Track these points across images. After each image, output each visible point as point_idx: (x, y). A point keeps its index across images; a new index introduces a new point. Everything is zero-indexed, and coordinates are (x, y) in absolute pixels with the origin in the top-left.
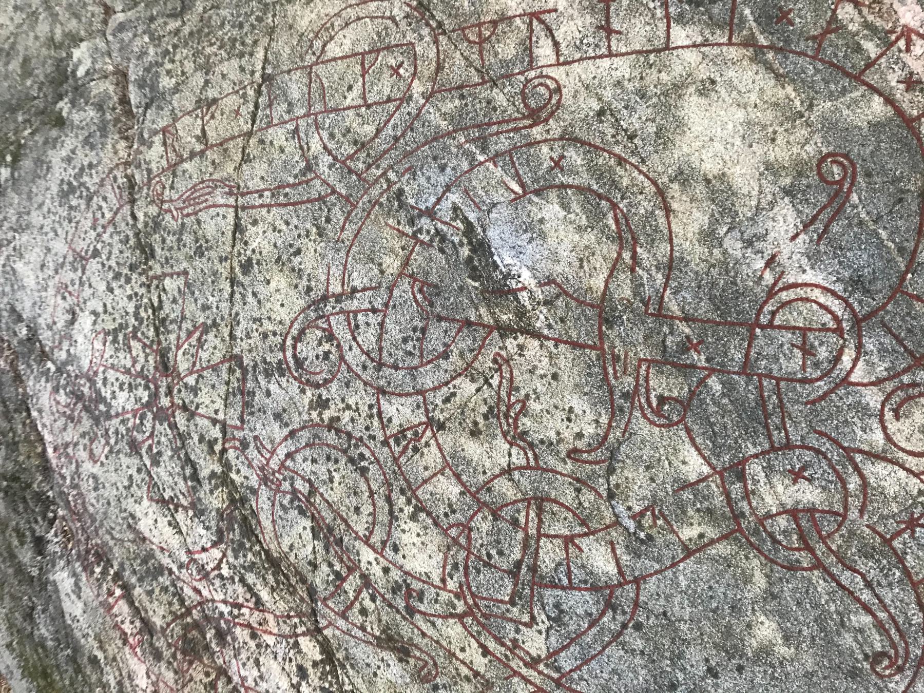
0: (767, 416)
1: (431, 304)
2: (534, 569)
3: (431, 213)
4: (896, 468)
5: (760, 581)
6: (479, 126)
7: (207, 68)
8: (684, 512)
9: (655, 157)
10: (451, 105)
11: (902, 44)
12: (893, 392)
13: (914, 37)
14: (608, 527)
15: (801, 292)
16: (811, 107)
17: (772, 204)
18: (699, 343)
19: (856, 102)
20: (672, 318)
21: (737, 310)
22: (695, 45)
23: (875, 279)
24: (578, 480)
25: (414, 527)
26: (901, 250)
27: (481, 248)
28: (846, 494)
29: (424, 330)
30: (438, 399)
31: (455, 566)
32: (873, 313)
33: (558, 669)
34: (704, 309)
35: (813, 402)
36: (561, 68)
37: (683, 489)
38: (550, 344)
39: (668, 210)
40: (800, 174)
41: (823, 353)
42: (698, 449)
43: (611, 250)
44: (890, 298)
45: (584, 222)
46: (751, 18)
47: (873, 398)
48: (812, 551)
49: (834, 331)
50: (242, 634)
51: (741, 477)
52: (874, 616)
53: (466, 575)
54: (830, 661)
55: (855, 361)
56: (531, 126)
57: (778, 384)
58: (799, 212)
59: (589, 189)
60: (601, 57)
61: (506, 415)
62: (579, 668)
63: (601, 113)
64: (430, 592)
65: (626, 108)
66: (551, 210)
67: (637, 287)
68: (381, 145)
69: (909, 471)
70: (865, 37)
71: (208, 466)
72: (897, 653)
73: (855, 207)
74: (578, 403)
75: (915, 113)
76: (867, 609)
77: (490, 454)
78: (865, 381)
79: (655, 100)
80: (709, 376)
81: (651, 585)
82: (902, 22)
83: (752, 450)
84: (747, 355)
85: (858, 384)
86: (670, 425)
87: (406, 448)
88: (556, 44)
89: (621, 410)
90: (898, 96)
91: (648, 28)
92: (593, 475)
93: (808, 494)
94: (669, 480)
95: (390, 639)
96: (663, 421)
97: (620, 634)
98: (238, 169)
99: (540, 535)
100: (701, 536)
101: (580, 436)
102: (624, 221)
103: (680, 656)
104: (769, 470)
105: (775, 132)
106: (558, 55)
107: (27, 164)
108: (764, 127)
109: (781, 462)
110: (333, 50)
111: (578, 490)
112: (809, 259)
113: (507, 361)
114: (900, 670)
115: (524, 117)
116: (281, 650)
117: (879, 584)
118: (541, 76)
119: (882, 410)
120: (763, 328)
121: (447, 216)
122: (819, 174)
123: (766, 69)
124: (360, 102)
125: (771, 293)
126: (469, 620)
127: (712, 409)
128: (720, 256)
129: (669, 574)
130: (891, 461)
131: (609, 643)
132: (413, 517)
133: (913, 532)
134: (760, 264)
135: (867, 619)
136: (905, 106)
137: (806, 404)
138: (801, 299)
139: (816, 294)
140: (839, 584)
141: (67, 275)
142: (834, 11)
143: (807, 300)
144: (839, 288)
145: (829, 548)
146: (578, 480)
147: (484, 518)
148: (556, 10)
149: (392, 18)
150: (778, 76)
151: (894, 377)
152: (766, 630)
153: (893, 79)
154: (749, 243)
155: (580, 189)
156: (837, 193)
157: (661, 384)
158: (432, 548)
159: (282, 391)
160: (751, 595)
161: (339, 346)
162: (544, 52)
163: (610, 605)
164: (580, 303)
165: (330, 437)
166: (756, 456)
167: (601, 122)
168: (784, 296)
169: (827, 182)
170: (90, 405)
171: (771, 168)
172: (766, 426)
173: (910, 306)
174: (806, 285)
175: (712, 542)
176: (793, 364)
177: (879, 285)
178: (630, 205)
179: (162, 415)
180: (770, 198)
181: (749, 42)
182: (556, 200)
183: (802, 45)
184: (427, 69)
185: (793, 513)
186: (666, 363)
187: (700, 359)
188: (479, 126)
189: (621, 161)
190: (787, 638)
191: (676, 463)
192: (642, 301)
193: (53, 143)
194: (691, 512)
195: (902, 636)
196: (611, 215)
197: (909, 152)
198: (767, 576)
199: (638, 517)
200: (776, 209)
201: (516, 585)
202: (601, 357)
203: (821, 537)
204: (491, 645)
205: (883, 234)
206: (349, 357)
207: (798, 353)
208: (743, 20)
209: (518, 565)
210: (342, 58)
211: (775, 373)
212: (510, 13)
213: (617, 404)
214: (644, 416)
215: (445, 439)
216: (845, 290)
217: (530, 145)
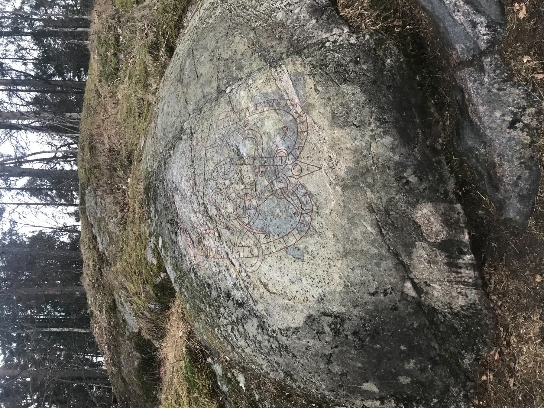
3: (232, 146)
5: (276, 202)
7: (203, 124)
10: (235, 126)
21: (273, 155)
25: (229, 203)
27: (239, 150)
30: (232, 179)
34: (267, 156)
41: (284, 160)
43: (255, 147)
47: (290, 167)
51: (273, 184)
66: (247, 142)
68: (225, 134)
71: (201, 201)
74: (250, 175)
77: (239, 187)
81: (261, 206)
93: (282, 185)
102: (256, 142)
107: (176, 149)
110: (220, 118)
121: (234, 145)
125: (277, 151)
139: (283, 150)
141: (181, 170)
155: (251, 138)
157: (262, 169)
159: (211, 183)
162: (248, 114)
165: (218, 190)
170: (184, 196)
171: (276, 130)
176: (279, 163)
179: (195, 194)
181: (275, 109)
184: (232, 120)
185: (280, 189)
187: (266, 164)
193: (180, 144)
199: (259, 194)
204: (241, 223)
215: (233, 186)
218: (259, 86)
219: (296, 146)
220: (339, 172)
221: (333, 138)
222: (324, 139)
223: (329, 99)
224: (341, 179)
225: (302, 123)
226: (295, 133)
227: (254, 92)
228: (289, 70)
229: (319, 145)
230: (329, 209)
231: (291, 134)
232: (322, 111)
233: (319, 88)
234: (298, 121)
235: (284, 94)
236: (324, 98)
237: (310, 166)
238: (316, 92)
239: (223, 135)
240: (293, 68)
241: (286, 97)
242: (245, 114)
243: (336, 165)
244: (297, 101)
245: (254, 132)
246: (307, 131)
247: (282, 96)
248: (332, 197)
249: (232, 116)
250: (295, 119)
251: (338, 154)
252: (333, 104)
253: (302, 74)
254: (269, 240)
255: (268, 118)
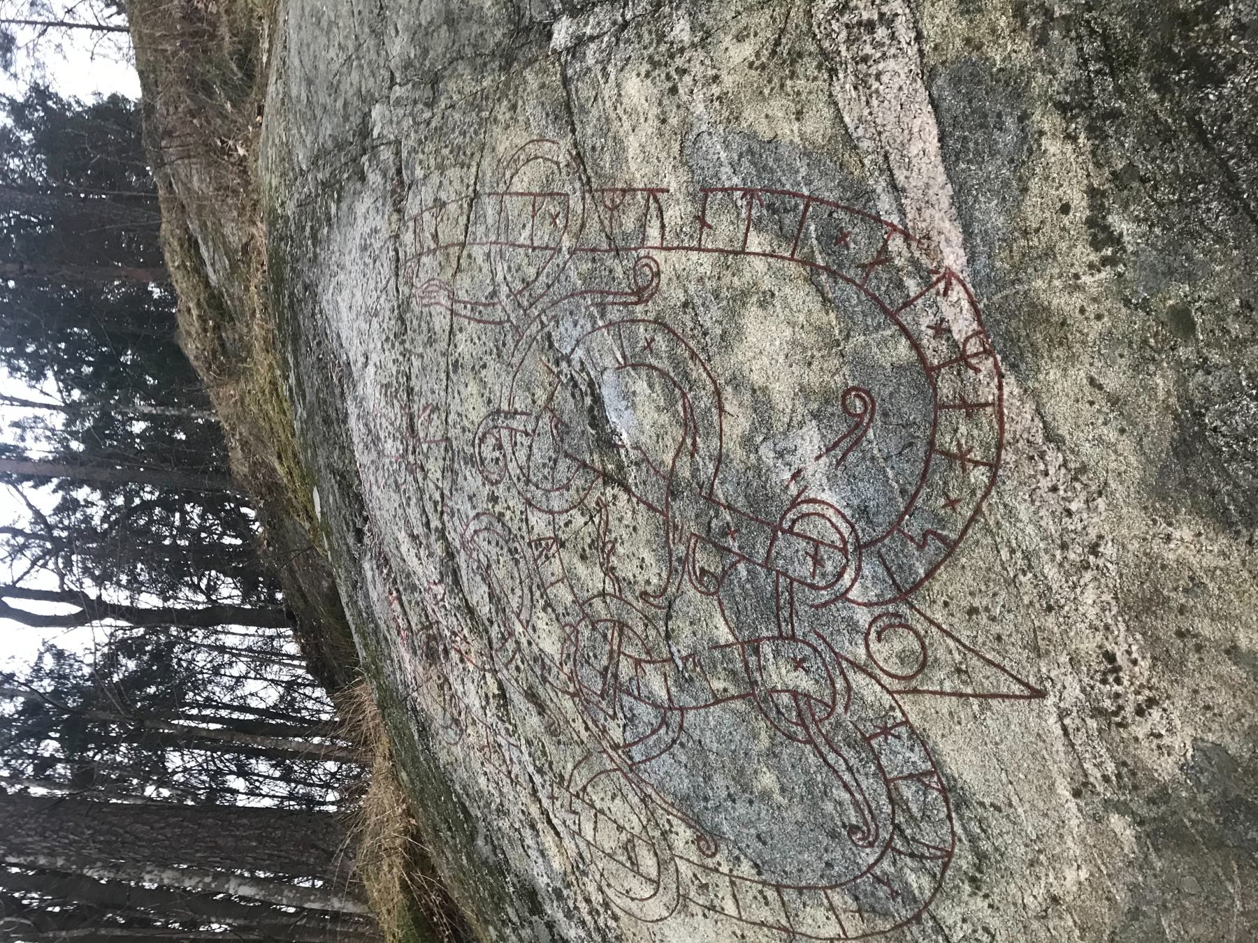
0: (779, 608)
1: (562, 440)
2: (615, 676)
4: (873, 681)
5: (764, 741)
6: (602, 292)
8: (715, 667)
9: (717, 357)
10: (586, 267)
11: (941, 286)
12: (880, 616)
13: (954, 282)
14: (664, 661)
15: (818, 508)
16: (848, 336)
17: (801, 425)
18: (736, 531)
19: (885, 341)
20: (719, 504)
21: (768, 513)
22: (764, 255)
23: (878, 513)
24: (646, 617)
26: (903, 492)
28: (834, 692)
29: (555, 461)
31: (568, 656)
32: (873, 543)
33: (631, 758)
34: (740, 503)
35: (817, 607)
36: (663, 253)
37: (715, 648)
38: (635, 500)
39: (721, 409)
40: (827, 402)
41: (829, 567)
42: (725, 620)
43: (679, 433)
44: (889, 533)
45: (662, 403)
46: (814, 235)
47: (863, 617)
48: (807, 728)
49: (840, 550)
50: (454, 656)
51: (756, 652)
52: (852, 794)
53: (575, 665)
54: (815, 818)
55: (854, 581)
56: (636, 303)
57: (791, 583)
58: (823, 436)
59: (668, 375)
60: (692, 249)
61: (601, 548)
62: (644, 762)
63: (685, 305)
64: (555, 670)
65: (703, 305)
67: (695, 471)
69: (883, 686)
70: (909, 274)
72: (869, 830)
73: (870, 442)
75: (936, 362)
76: (846, 786)
77: (592, 578)
78: (860, 600)
79: (725, 303)
80: (739, 561)
82: (946, 263)
83: (765, 634)
84: (769, 552)
85: (853, 602)
86: (708, 594)
87: (541, 553)
88: (663, 227)
89: (676, 571)
90: (925, 341)
91: (731, 228)
92: (655, 616)
93: (805, 683)
94: (706, 638)
95: (533, 695)
96: (703, 589)
97: (671, 746)
98: (454, 275)
99: (620, 653)
100: (725, 690)
101: (648, 582)
103: (710, 777)
104: (777, 653)
105: (813, 357)
106: (663, 238)
108: (805, 349)
109: (788, 649)
111: (646, 626)
112: (829, 479)
113: (605, 506)
114: (871, 845)
115: (633, 293)
116: (476, 676)
117: (858, 771)
118: (647, 257)
119: (869, 629)
120: (784, 532)
122: (843, 404)
123: (818, 290)
124: (529, 242)
125: (794, 503)
126: (577, 700)
127: (737, 590)
128: (754, 461)
129: (702, 711)
130: (871, 675)
131: (664, 751)
132: (544, 609)
133: (886, 739)
134: (787, 476)
135: (847, 796)
136: (929, 353)
137: (812, 606)
138: (818, 514)
140: (825, 760)
142: (886, 241)
143: (823, 516)
144: (848, 512)
145: (820, 731)
146: (646, 617)
147: (586, 626)
148: (668, 191)
149: (557, 163)
150: (825, 300)
151: (882, 604)
152: (768, 780)
153: (926, 321)
154: (780, 455)
156: (857, 426)
157: (703, 559)
158: (555, 637)
160: (757, 749)
161: (504, 456)
162: (653, 232)
163: (664, 722)
164: (657, 472)
166: (768, 639)
167: (685, 313)
168: (805, 508)
169: (850, 414)
171: (804, 392)
172: (777, 617)
173: (904, 545)
174: (823, 502)
175: (733, 697)
176: (804, 569)
177: (880, 519)
178: (695, 397)
180: (800, 418)
181: (808, 262)
182: (645, 378)
183: (852, 272)
185: (794, 694)
186: (710, 541)
187: (734, 545)
188: (602, 292)
189: (694, 356)
190: (783, 790)
191: (711, 626)
192: (698, 483)
194: (719, 669)
195: (873, 818)
196: (680, 403)
197: (924, 400)
198: (770, 737)
200: (804, 429)
201: (604, 684)
202: (666, 522)
203: (814, 719)
204: (590, 724)
205: (890, 473)
206: (510, 466)
207: (810, 561)
208: (807, 237)
209: (606, 669)
210: (522, 194)
211: (790, 573)
212: (635, 186)
213: (675, 566)
214: (691, 581)
216: (853, 516)
217: (633, 321)
218: (728, 81)
219: (914, 526)
220: (1146, 753)
221: (1153, 562)
222: (1094, 549)
223: (1182, 321)
224: (1149, 790)
225: (971, 409)
226: (920, 443)
227: (699, 108)
228: (929, 29)
229: (1051, 572)
230: (1040, 891)
231: (893, 446)
232: (1113, 381)
233: (1119, 223)
234: (946, 389)
235: (881, 185)
236: (1144, 305)
237: (975, 661)
238: (1096, 245)
239: (527, 284)
240: (961, 25)
241: (885, 204)
242: (643, 226)
243: (1140, 712)
244: (954, 258)
245: (681, 350)
246: (994, 466)
247: (870, 195)
248: (1075, 849)
249: (575, 203)
250: (930, 372)
251: (1163, 660)
252: (1205, 366)
253: (1014, 86)
254: (710, 862)
255: (766, 301)
